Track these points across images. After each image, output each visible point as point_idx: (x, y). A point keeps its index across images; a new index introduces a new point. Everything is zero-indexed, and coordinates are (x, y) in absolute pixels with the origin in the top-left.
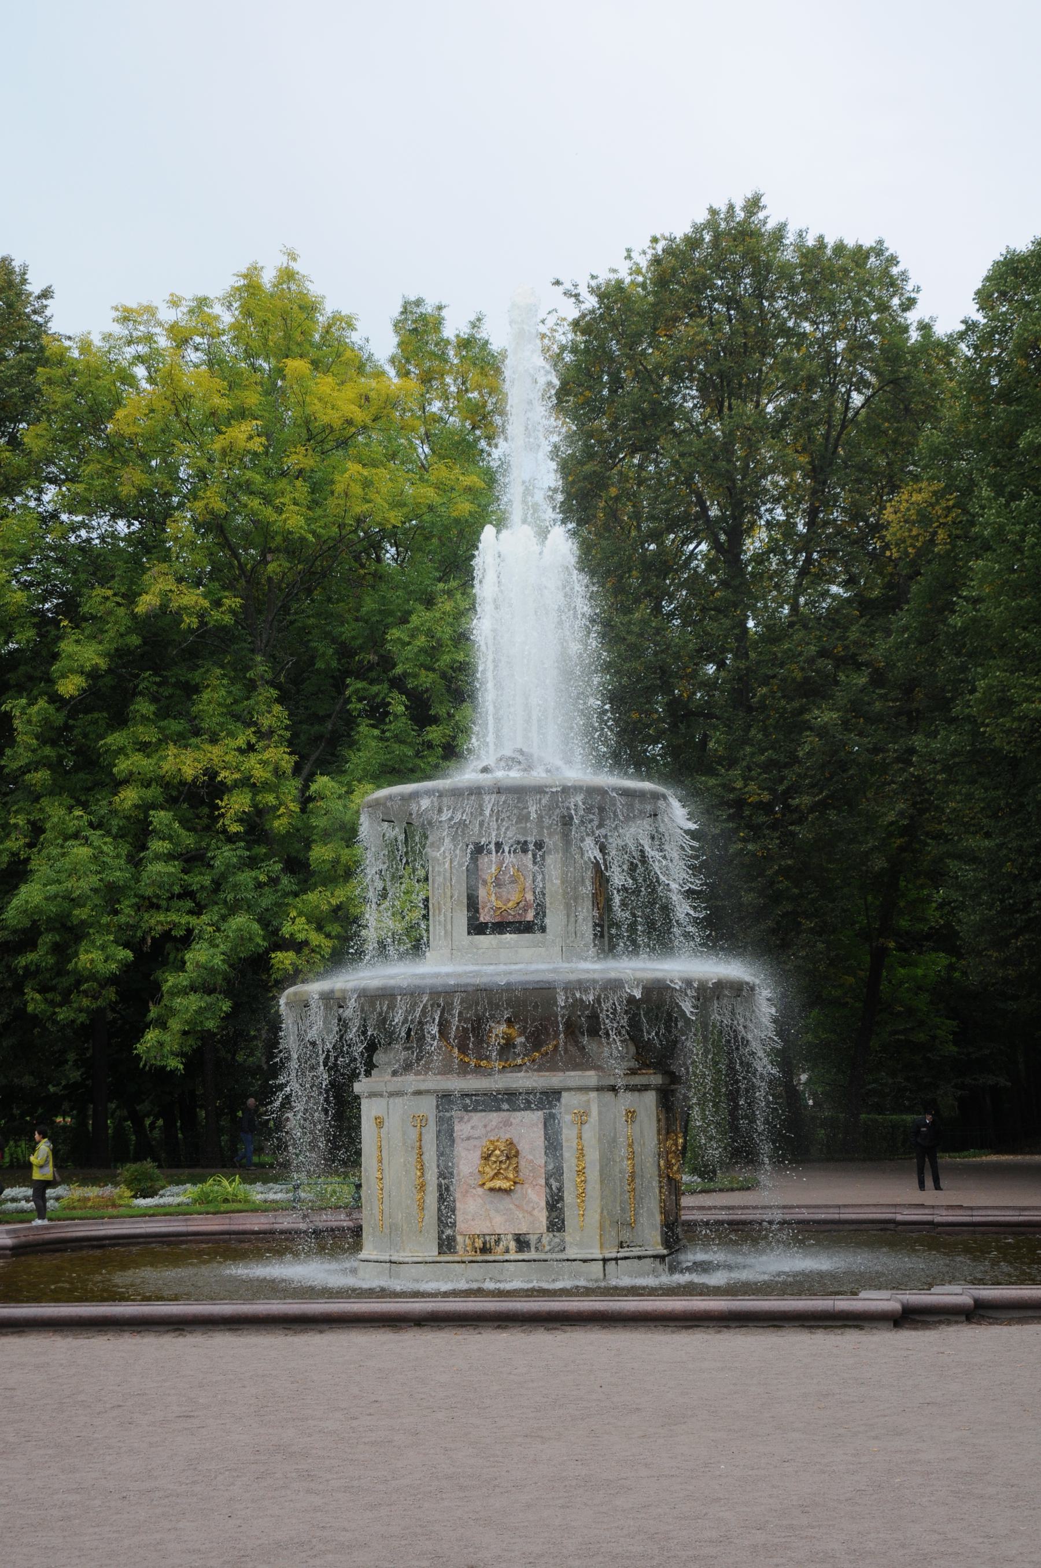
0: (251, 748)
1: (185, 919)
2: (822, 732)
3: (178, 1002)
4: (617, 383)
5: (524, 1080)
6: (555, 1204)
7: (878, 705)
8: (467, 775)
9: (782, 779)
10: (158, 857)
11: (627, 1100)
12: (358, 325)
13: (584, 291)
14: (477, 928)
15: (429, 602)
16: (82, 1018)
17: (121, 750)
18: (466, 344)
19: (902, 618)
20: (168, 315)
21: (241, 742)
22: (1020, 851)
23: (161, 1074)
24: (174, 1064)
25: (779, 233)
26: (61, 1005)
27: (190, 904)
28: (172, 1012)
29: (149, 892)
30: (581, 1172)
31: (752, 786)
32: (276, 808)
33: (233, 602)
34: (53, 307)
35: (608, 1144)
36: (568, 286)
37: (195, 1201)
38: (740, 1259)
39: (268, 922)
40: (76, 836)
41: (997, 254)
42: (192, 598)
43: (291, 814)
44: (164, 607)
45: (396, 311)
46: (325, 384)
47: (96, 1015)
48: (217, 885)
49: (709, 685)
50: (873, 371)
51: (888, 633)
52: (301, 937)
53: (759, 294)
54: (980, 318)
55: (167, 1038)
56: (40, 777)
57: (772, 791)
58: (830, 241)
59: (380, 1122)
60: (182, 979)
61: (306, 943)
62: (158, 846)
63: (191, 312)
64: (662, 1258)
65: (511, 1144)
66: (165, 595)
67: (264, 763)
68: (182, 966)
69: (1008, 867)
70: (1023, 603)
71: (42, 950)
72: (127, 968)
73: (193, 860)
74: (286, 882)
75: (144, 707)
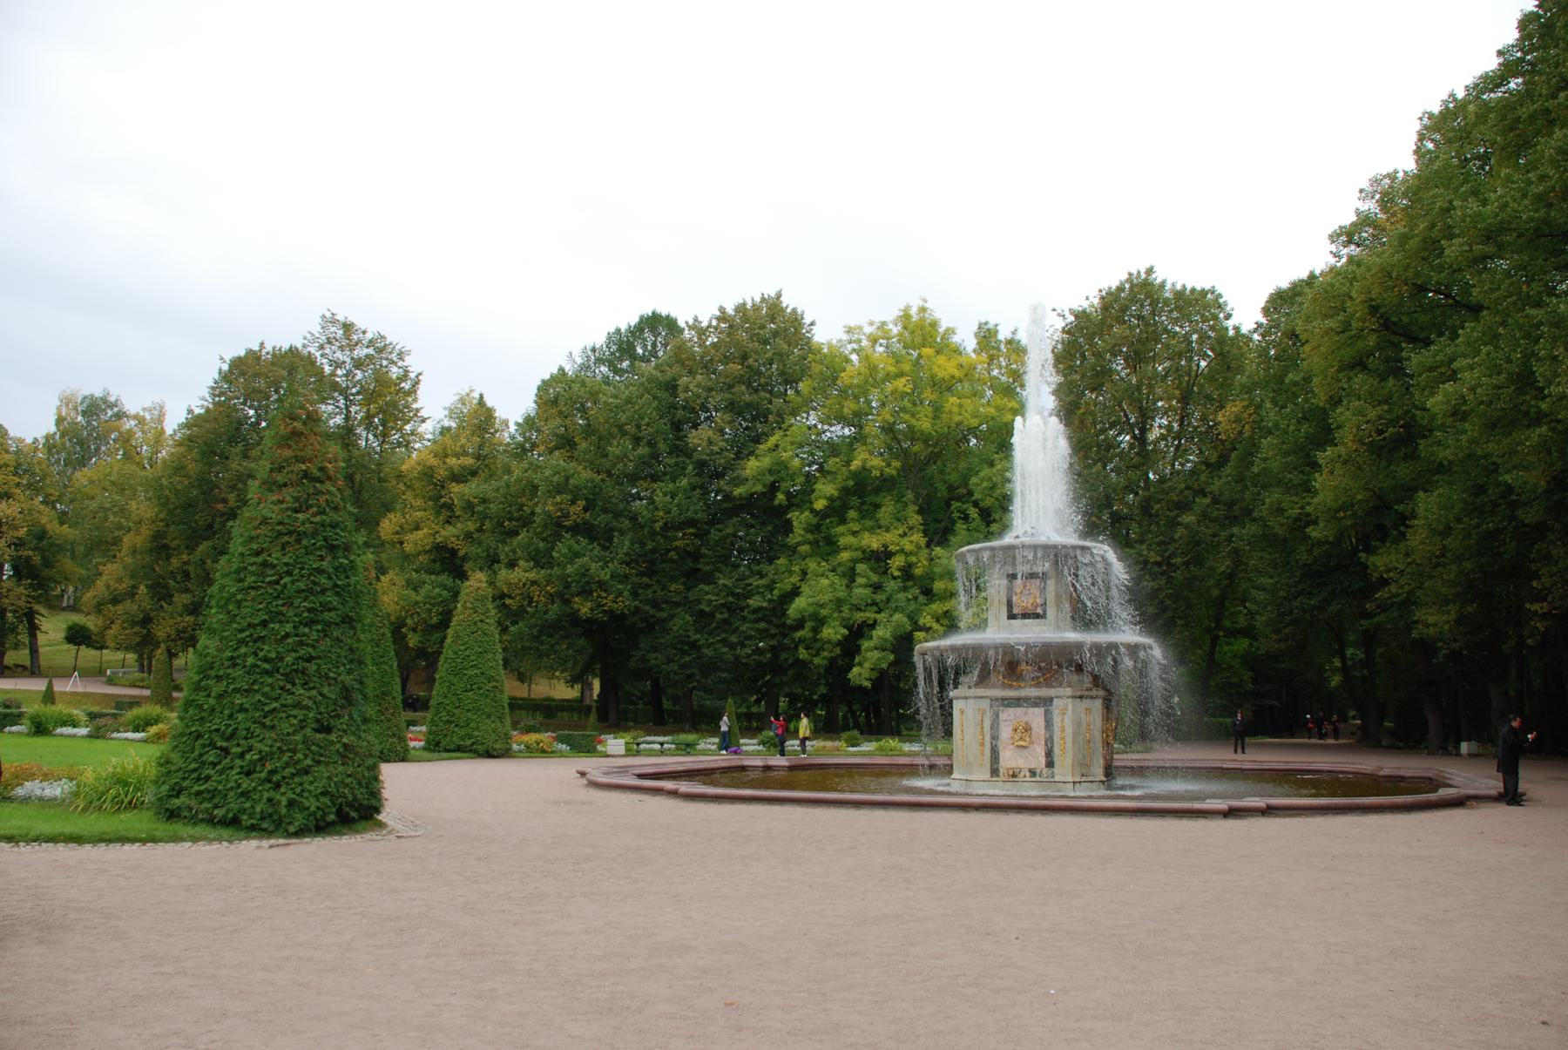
0: (905, 534)
1: (873, 616)
2: (1187, 527)
3: (869, 655)
4: (1083, 357)
5: (1033, 692)
6: (1049, 754)
7: (1216, 513)
8: (1008, 539)
9: (1167, 550)
10: (860, 586)
11: (1087, 703)
12: (958, 332)
13: (1067, 313)
14: (1012, 616)
15: (992, 464)
16: (825, 662)
17: (842, 534)
18: (1009, 342)
19: (1228, 470)
20: (868, 330)
21: (900, 532)
22: (1287, 584)
23: (860, 688)
24: (867, 684)
25: (1162, 285)
26: (815, 656)
27: (876, 609)
28: (866, 659)
29: (856, 603)
30: (1062, 738)
31: (1152, 553)
32: (916, 563)
33: (896, 464)
34: (815, 329)
35: (1078, 724)
36: (1059, 311)
37: (876, 750)
38: (1150, 784)
39: (912, 618)
40: (823, 575)
41: (1271, 290)
42: (876, 462)
43: (924, 566)
44: (864, 468)
45: (975, 328)
46: (941, 360)
47: (832, 660)
48: (888, 600)
49: (1130, 507)
50: (1212, 350)
51: (1220, 478)
52: (928, 625)
53: (1153, 313)
54: (1264, 321)
55: (863, 671)
56: (805, 548)
57: (1163, 556)
58: (1189, 287)
59: (962, 712)
60: (871, 644)
61: (930, 628)
62: (861, 580)
63: (878, 328)
64: (1103, 782)
65: (1027, 723)
66: (865, 461)
67: (911, 542)
68: (871, 638)
69: (1281, 593)
70: (1289, 459)
71: (807, 630)
72: (846, 638)
73: (877, 587)
74: (922, 599)
75: (852, 514)
